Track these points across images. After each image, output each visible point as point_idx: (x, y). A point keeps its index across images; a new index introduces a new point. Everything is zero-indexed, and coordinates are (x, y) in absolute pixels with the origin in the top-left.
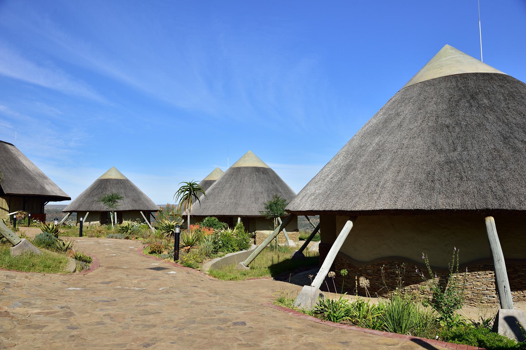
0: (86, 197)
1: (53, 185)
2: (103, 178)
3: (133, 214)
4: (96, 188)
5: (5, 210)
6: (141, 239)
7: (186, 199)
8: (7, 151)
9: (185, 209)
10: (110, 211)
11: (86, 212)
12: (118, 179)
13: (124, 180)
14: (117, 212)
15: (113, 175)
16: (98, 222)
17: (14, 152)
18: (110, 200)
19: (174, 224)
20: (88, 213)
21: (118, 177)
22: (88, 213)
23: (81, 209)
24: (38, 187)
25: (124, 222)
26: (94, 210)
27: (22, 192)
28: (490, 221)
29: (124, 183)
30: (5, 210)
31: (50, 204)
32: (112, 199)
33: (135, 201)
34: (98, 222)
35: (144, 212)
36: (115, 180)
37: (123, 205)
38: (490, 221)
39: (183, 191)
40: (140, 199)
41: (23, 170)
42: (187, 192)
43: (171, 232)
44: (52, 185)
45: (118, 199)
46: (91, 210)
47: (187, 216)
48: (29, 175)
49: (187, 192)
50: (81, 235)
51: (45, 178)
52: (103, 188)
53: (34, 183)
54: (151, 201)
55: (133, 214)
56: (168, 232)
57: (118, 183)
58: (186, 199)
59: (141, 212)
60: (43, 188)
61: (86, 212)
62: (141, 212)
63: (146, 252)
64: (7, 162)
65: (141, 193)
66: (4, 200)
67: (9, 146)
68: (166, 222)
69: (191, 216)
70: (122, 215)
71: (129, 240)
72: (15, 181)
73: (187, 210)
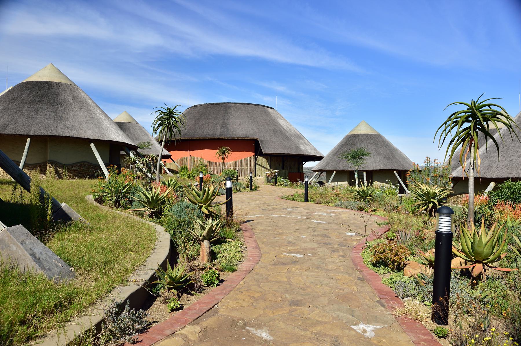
0: (334, 155)
1: (309, 144)
2: (352, 133)
3: (384, 174)
4: (344, 145)
5: (266, 169)
6: (381, 213)
7: (463, 140)
8: (267, 114)
9: (460, 162)
10: (353, 171)
11: (333, 171)
12: (368, 134)
13: (375, 135)
14: (367, 171)
15: (363, 130)
16: (347, 182)
17: (276, 116)
18: (354, 157)
19: (437, 191)
20: (335, 172)
21: (368, 131)
22: (335, 172)
23: (328, 168)
24: (293, 146)
25: (374, 183)
26: (341, 169)
27: (278, 152)
28: (364, 173)
29: (375, 139)
30: (266, 169)
31: (308, 165)
32: (357, 156)
33: (388, 159)
34: (347, 182)
35: (400, 172)
36: (365, 134)
37: (372, 163)
38: (364, 173)
39: (456, 123)
40: (394, 156)
41: (281, 131)
42: (466, 125)
43: (431, 205)
44: (307, 145)
45: (363, 155)
46: (338, 169)
47: (467, 179)
48: (286, 136)
49: (466, 125)
50: (306, 200)
51: (300, 137)
52: (352, 145)
53: (289, 142)
54: (407, 159)
55: (384, 174)
56: (426, 204)
57: (368, 138)
58: (463, 140)
59: (395, 172)
60: (298, 148)
61: (333, 171)
62: (395, 172)
63: (368, 257)
64: (267, 124)
65: (395, 150)
66: (265, 160)
67: (270, 109)
68: (424, 187)
69: (476, 179)
70: (373, 175)
71: (363, 213)
72: (273, 142)
73: (466, 164)
